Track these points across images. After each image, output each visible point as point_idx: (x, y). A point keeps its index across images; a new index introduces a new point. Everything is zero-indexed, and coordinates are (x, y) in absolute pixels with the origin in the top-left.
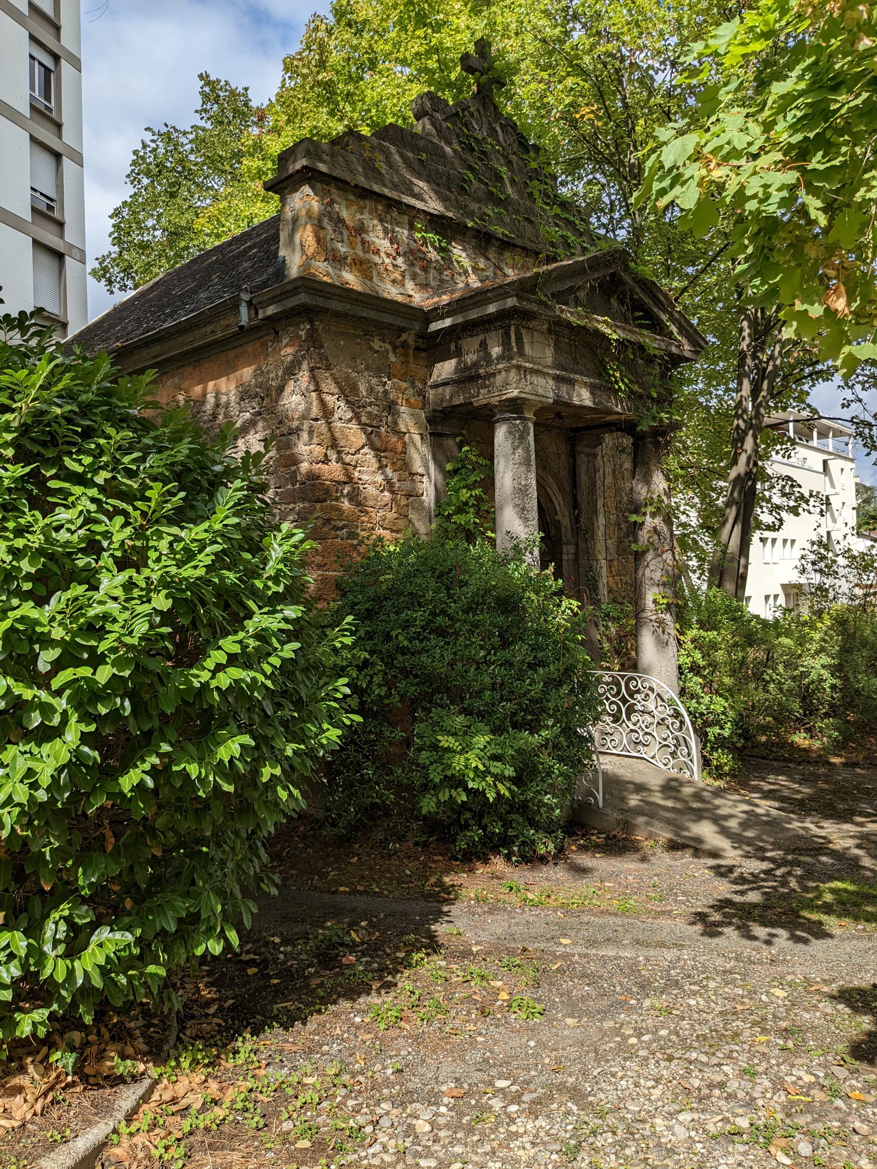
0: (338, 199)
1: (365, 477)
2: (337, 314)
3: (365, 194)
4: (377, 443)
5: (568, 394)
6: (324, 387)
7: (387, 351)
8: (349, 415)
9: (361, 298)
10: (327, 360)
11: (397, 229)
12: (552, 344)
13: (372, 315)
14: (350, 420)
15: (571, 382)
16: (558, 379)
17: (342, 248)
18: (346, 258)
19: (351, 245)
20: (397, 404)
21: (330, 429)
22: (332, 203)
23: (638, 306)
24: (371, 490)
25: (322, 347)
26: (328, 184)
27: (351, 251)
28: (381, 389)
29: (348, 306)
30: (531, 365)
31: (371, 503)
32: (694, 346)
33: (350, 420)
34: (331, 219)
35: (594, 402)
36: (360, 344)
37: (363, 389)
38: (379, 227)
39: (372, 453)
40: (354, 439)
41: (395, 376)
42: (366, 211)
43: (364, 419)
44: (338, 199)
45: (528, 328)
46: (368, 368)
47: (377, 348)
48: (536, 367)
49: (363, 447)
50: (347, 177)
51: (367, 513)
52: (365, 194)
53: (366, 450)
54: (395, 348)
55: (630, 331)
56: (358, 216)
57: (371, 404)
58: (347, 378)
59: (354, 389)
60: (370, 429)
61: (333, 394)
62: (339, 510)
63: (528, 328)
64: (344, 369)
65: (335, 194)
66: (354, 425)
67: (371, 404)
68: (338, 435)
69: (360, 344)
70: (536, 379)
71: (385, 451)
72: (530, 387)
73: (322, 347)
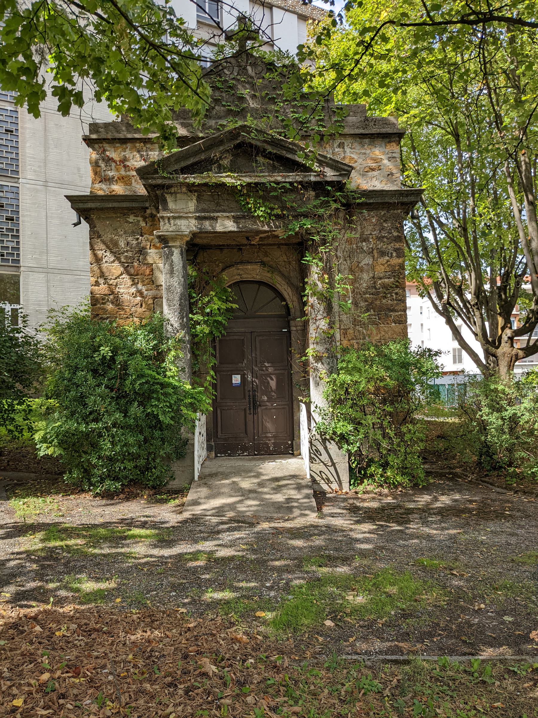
0: (109, 149)
1: (122, 291)
2: (97, 209)
3: (124, 141)
4: (132, 271)
5: (211, 226)
6: (96, 247)
7: (139, 221)
8: (112, 259)
9: (104, 198)
10: (98, 233)
11: (150, 153)
12: (195, 198)
13: (116, 205)
14: (114, 261)
15: (215, 219)
16: (198, 218)
17: (110, 174)
18: (114, 178)
19: (117, 170)
20: (146, 249)
21: (100, 268)
22: (104, 151)
23: (280, 159)
24: (126, 297)
25: (95, 227)
26: (101, 143)
27: (117, 173)
28: (135, 242)
29: (99, 204)
30: (172, 214)
31: (127, 304)
32: (338, 171)
33: (114, 261)
34: (103, 160)
35: (238, 227)
36: (119, 221)
37: (122, 244)
38: (138, 155)
39: (128, 277)
40: (115, 271)
41: (145, 234)
42: (128, 150)
43: (123, 260)
44: (109, 149)
45: (170, 193)
46: (125, 233)
47: (131, 220)
48: (176, 215)
49: (121, 274)
50: (118, 136)
51: (123, 309)
52: (124, 141)
53: (124, 276)
54: (145, 219)
55: (254, 176)
56: (123, 153)
57: (127, 251)
58: (112, 240)
59: (116, 244)
60: (126, 265)
61: (101, 250)
62: (105, 310)
63: (170, 193)
64: (108, 236)
65: (106, 146)
66: (116, 264)
67: (127, 251)
68: (105, 270)
69: (119, 221)
70: (178, 222)
71: (136, 275)
72: (174, 228)
73: (95, 227)
